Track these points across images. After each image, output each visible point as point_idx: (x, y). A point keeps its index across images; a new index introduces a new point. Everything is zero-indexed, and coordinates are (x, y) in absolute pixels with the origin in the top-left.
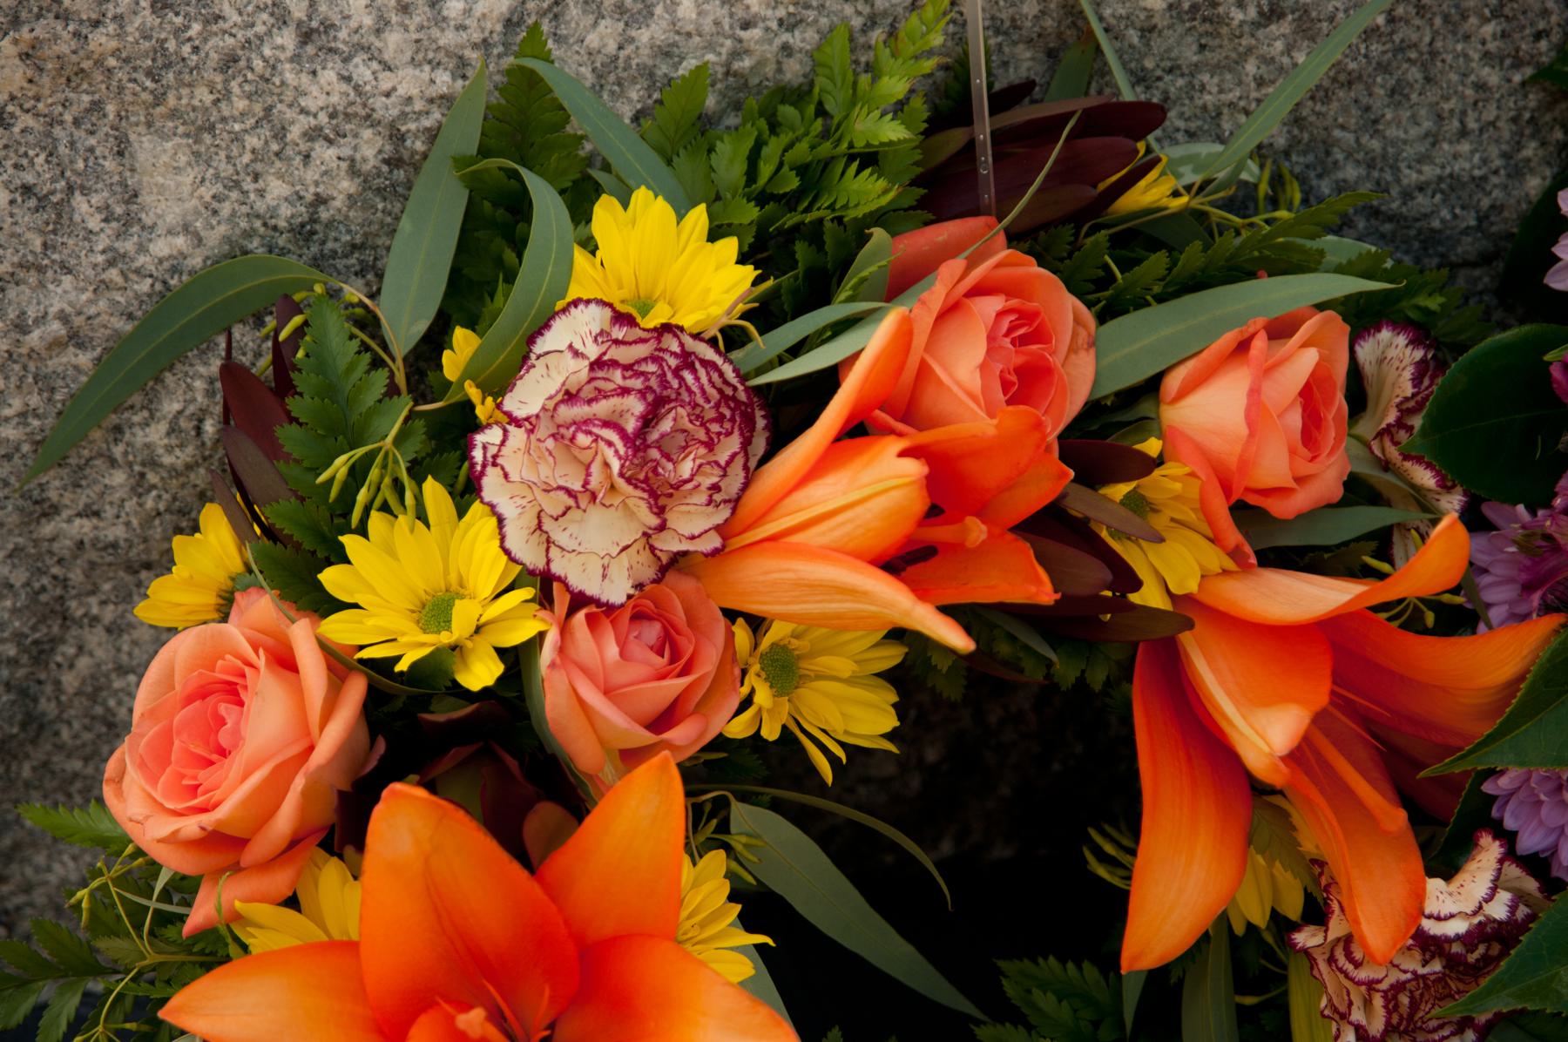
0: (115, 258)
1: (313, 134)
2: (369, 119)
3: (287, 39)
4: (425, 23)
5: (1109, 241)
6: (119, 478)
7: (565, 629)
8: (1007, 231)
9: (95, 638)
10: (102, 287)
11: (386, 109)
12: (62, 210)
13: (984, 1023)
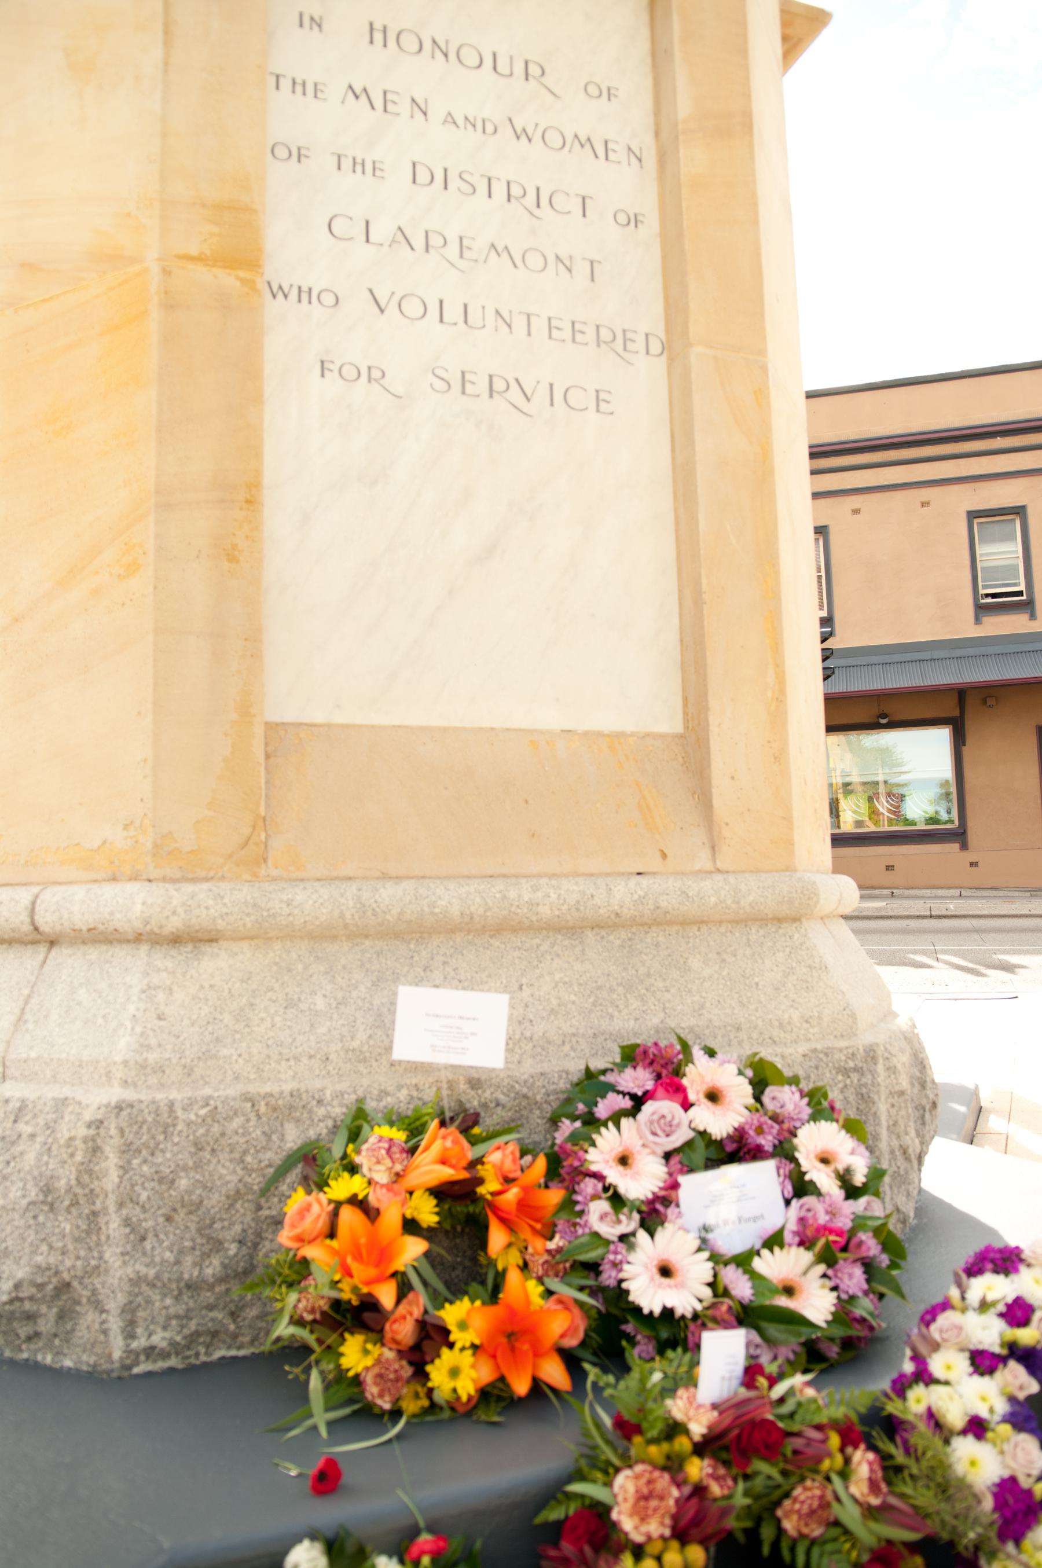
0: (280, 1147)
1: (320, 1120)
2: (330, 1117)
3: (315, 1103)
4: (70, 1151)
5: (1016, 1270)
6: (276, 1200)
7: (374, 1191)
8: (458, 1128)
9: (267, 1243)
10: (277, 1153)
11: (333, 1115)
12: (270, 1137)
13: (487, 1290)
